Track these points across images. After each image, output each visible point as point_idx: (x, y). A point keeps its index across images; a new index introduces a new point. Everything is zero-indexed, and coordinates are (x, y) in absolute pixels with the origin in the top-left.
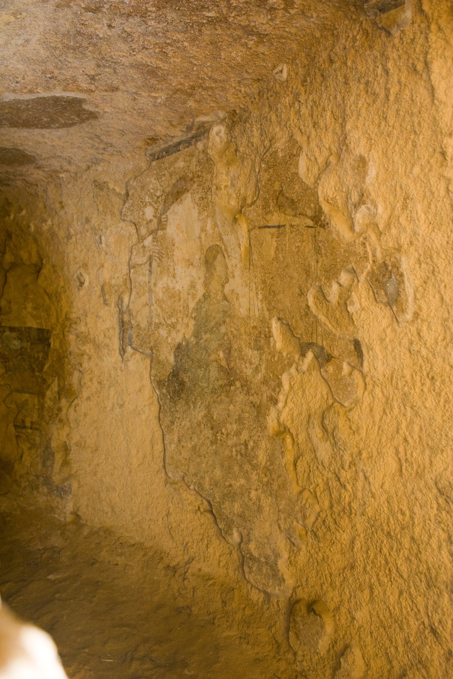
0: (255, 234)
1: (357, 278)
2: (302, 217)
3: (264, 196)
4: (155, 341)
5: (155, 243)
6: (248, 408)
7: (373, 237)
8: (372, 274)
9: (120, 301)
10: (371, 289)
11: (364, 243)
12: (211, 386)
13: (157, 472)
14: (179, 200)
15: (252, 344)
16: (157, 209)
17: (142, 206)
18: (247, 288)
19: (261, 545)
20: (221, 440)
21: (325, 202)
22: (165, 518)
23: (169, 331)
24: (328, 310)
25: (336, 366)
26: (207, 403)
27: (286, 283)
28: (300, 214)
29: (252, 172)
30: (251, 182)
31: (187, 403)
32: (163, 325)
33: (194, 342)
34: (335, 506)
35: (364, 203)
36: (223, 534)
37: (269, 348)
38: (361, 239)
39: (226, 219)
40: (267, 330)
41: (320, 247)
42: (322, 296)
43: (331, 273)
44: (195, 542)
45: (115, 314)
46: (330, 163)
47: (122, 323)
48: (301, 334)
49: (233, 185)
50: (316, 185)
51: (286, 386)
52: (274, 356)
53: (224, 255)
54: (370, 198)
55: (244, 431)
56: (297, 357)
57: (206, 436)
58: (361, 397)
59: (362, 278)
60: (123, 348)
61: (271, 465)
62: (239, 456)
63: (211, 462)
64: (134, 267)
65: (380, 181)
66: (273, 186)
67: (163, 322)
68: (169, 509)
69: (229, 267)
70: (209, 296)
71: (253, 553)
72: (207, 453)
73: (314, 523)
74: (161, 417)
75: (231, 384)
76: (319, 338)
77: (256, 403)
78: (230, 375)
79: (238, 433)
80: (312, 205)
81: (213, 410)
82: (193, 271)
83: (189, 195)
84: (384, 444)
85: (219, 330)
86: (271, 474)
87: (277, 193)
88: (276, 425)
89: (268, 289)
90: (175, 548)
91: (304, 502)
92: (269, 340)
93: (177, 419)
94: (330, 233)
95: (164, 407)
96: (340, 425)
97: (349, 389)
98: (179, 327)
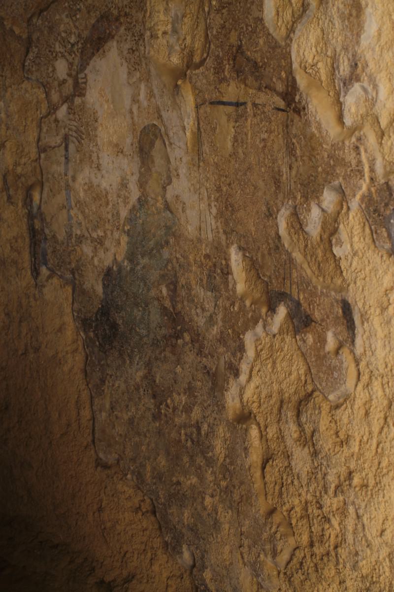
0: (206, 112)
1: (347, 203)
2: (268, 91)
3: (217, 53)
4: (77, 261)
5: (71, 116)
6: (200, 376)
7: (372, 139)
8: (368, 200)
9: (28, 200)
10: (367, 223)
11: (357, 148)
12: (152, 336)
13: (86, 448)
14: (101, 51)
15: (205, 282)
16: (71, 64)
17: (51, 57)
18: (197, 196)
19: (219, 578)
20: (166, 415)
21: (302, 71)
22: (96, 514)
23: (95, 248)
24: (306, 246)
25: (317, 335)
26: (147, 359)
27: (248, 194)
28: (266, 88)
29: (201, 12)
30: (199, 28)
31: (121, 355)
32: (87, 238)
33: (128, 268)
34: (317, 544)
35: (358, 80)
36: (172, 548)
37: (227, 290)
38: (354, 139)
39: (165, 86)
40: (224, 262)
41: (293, 144)
42: (298, 224)
43: (310, 190)
44: (136, 553)
45: (23, 216)
46: (308, 5)
47: (34, 233)
48: (270, 277)
49: (175, 31)
50: (288, 42)
51: (250, 353)
52: (233, 304)
53: (164, 141)
54: (368, 70)
55: (196, 408)
56: (264, 310)
57: (147, 406)
58: (352, 390)
59: (355, 203)
60: (35, 268)
61: (231, 463)
62: (189, 443)
63: (153, 445)
64: (44, 151)
65: (383, 42)
66: (229, 39)
67: (87, 234)
68: (101, 501)
69: (172, 160)
70: (147, 202)
71: (209, 586)
72: (148, 430)
73: (288, 563)
74: (88, 371)
75: (178, 336)
76: (294, 287)
77: (211, 369)
78: (176, 321)
79: (188, 409)
80: (283, 75)
81: (155, 369)
82: (124, 162)
83: (115, 44)
84: (385, 471)
85: (160, 254)
86: (231, 477)
87: (234, 49)
88: (238, 405)
89: (224, 201)
90: (111, 557)
91: (273, 530)
92: (227, 279)
93: (108, 377)
94: (307, 123)
95: (91, 357)
96: (322, 428)
97: (336, 375)
98: (107, 243)
